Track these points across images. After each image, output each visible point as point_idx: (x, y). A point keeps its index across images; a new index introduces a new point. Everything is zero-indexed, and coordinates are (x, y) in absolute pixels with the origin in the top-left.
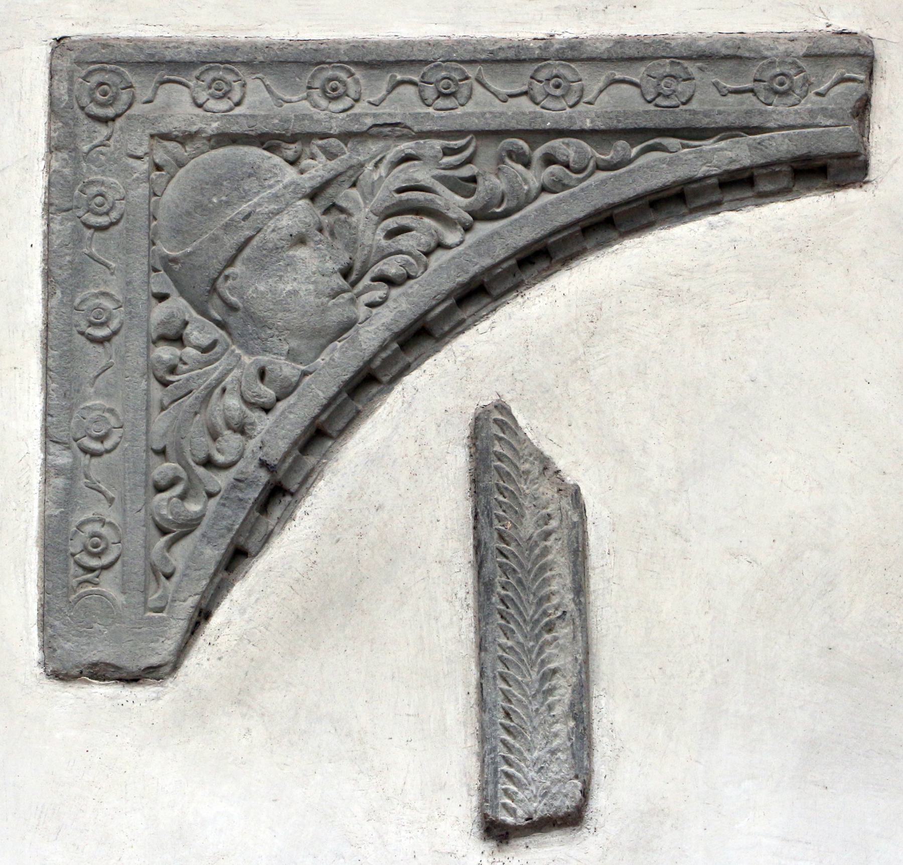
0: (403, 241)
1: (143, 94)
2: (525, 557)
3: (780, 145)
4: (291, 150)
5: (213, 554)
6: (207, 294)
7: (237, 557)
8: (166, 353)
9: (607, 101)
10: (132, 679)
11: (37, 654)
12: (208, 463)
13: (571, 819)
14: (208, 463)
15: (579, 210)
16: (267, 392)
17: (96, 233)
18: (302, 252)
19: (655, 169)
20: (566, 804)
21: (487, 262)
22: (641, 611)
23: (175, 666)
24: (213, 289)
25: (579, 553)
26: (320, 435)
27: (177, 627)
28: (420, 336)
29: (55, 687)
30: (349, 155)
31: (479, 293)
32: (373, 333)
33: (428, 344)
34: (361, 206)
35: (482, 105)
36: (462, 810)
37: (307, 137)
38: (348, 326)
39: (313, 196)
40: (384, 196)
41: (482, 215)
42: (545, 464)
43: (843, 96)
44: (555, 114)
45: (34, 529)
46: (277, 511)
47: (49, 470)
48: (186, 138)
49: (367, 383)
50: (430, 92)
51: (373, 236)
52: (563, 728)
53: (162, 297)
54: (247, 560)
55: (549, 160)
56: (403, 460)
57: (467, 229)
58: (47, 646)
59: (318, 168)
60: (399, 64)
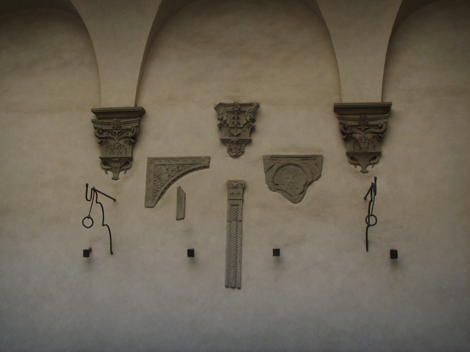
0: (173, 173)
1: (154, 162)
2: (181, 198)
3: (202, 165)
4: (165, 166)
5: (157, 198)
6: (158, 178)
7: (159, 198)
8: (155, 182)
9: (190, 162)
10: (151, 208)
11: (144, 206)
12: (157, 191)
13: (183, 219)
14: (157, 191)
15: (187, 171)
16: (162, 185)
17: (133, 105)
18: (166, 174)
19: (193, 167)
20: (182, 218)
21: (179, 175)
22: (190, 202)
23: (154, 206)
24: (159, 177)
25: (185, 198)
26: (166, 188)
27: (155, 203)
28: (174, 181)
29: (146, 208)
30: (170, 166)
31: (179, 177)
32: (170, 181)
33: (171, 185)
34: (170, 170)
35: (180, 162)
36: (175, 218)
37: (166, 165)
38: (168, 180)
39: (167, 169)
40: (172, 170)
41: (179, 171)
42: (183, 191)
43: (208, 161)
44: (185, 163)
45: (145, 196)
46: (163, 194)
47: (146, 191)
48: (157, 165)
49: (170, 184)
50: (176, 161)
51: (171, 173)
52: (183, 212)
53: (155, 178)
54: (382, 153)
55: (185, 166)
56: (172, 190)
57: (178, 172)
58: (145, 205)
59: (167, 167)
60: (174, 159)
